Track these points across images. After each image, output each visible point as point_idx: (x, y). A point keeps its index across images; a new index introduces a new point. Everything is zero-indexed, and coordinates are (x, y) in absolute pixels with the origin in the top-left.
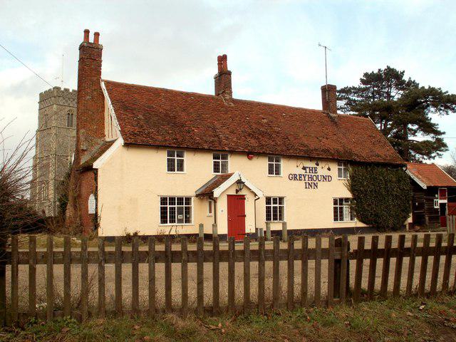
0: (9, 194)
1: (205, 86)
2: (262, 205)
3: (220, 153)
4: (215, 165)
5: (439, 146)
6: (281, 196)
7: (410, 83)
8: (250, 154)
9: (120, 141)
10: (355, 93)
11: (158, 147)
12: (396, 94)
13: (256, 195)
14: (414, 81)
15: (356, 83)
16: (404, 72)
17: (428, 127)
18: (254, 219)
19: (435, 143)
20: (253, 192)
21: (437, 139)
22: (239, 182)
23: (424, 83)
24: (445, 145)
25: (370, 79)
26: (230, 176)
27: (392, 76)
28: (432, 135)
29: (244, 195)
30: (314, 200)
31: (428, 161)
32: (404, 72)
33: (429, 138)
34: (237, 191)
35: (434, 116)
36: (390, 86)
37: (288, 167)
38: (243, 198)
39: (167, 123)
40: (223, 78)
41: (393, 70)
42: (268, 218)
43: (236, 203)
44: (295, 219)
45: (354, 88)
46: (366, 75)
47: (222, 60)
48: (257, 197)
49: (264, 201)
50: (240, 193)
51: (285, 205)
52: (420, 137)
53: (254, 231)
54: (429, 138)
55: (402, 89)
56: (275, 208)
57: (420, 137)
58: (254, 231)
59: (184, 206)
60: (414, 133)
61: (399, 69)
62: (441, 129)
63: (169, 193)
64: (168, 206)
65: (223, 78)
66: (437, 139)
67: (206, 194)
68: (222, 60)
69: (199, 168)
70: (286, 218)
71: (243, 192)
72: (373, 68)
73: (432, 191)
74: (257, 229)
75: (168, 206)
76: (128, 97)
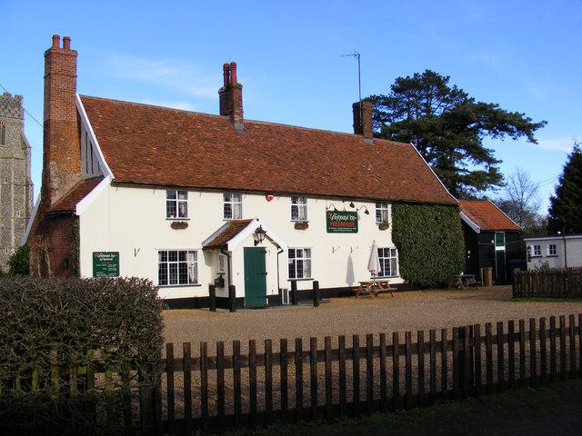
0: (560, 188)
1: (206, 101)
2: (285, 261)
3: (232, 191)
4: (225, 209)
5: (494, 178)
6: (307, 246)
7: (457, 94)
8: (269, 193)
9: (109, 177)
10: (383, 104)
11: (155, 186)
12: (438, 108)
13: (279, 247)
14: (461, 91)
15: (386, 91)
16: (448, 77)
17: (481, 154)
18: (277, 279)
19: (488, 175)
20: (275, 244)
21: (491, 169)
22: (260, 231)
23: (480, 94)
24: (500, 177)
25: (403, 86)
26: (247, 223)
27: (431, 83)
28: (485, 164)
29: (264, 248)
30: (345, 250)
31: (479, 194)
32: (448, 77)
33: (482, 167)
34: (256, 243)
35: (487, 141)
36: (429, 97)
37: (317, 209)
38: (263, 251)
39: (157, 150)
40: (230, 95)
41: (434, 75)
42: (292, 274)
43: (255, 259)
44: (327, 274)
45: (384, 98)
46: (399, 80)
47: (229, 70)
48: (280, 250)
49: (286, 253)
50: (259, 245)
51: (313, 258)
52: (469, 165)
53: (276, 293)
54: (482, 167)
55: (447, 101)
56: (300, 262)
57: (469, 165)
58: (276, 293)
59: (178, 262)
60: (461, 157)
61: (443, 73)
62: (496, 156)
63: (169, 247)
64: (169, 263)
65: (230, 95)
66: (491, 169)
67: (217, 247)
68: (229, 70)
69: (206, 211)
70: (315, 276)
71: (265, 243)
72: (407, 73)
73: (488, 234)
74: (280, 290)
75: (169, 263)
76: (111, 115)
